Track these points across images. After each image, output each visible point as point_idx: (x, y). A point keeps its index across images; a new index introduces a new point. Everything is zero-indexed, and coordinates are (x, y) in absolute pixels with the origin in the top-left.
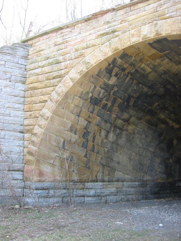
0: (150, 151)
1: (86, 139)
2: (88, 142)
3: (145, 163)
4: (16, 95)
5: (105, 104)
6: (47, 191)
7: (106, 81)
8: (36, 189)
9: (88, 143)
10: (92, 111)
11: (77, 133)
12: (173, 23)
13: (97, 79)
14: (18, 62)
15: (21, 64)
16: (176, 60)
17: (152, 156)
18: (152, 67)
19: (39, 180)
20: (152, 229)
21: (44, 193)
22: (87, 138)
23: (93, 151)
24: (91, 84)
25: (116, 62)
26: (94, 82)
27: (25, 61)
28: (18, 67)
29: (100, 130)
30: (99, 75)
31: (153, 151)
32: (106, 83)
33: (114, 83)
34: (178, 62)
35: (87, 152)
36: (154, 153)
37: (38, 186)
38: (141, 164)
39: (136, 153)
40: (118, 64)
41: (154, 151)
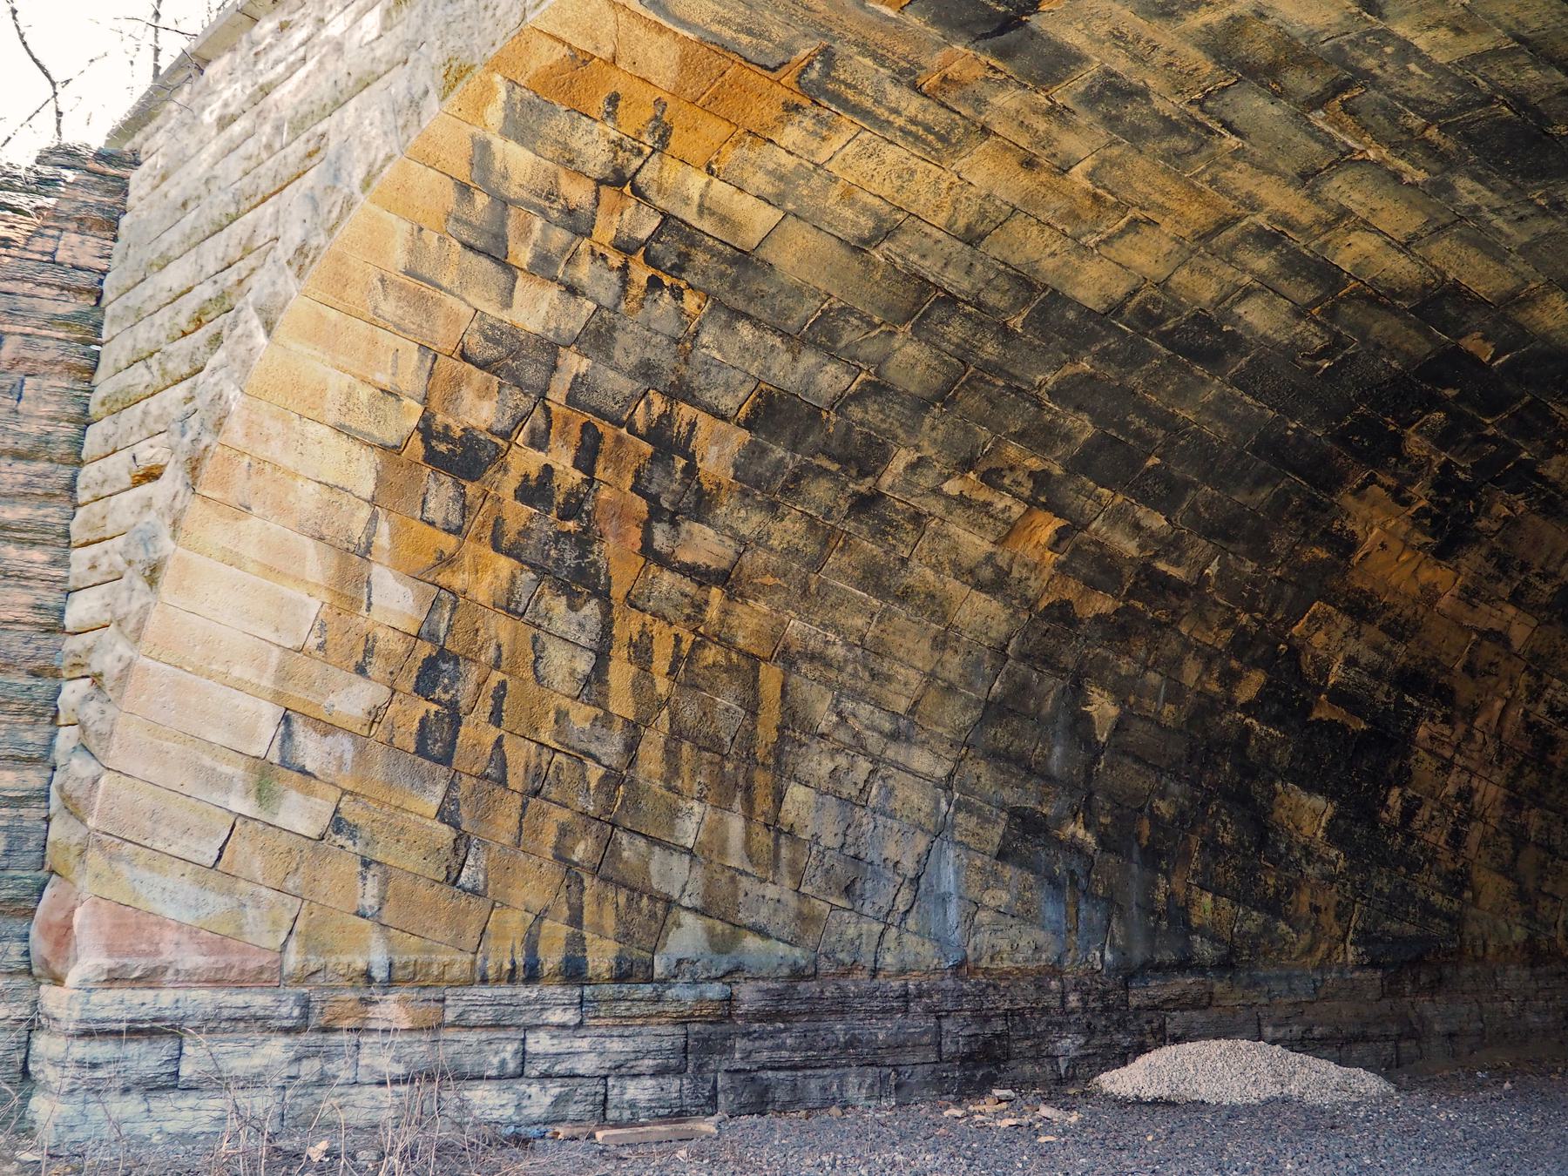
0: (914, 774)
1: (438, 702)
2: (460, 723)
3: (891, 851)
4: (24, 445)
5: (534, 474)
6: (167, 1046)
7: (492, 310)
8: (87, 1034)
9: (462, 729)
10: (455, 519)
11: (376, 668)
12: (1208, 96)
13: (423, 297)
14: (52, 254)
15: (75, 267)
16: (913, 121)
17: (938, 802)
18: (769, 191)
19: (110, 971)
20: (1544, 947)
21: (147, 1058)
22: (447, 697)
23: (502, 781)
24: (387, 339)
25: (498, 165)
26: (407, 324)
27: (103, 248)
28: (49, 285)
29: (535, 639)
30: (425, 271)
31: (940, 772)
32: (492, 327)
33: (553, 325)
34: (935, 134)
35: (452, 785)
36: (947, 785)
37: (98, 1016)
38: (856, 857)
39: (817, 790)
40: (517, 178)
41: (951, 775)
